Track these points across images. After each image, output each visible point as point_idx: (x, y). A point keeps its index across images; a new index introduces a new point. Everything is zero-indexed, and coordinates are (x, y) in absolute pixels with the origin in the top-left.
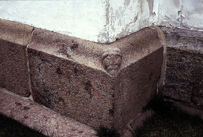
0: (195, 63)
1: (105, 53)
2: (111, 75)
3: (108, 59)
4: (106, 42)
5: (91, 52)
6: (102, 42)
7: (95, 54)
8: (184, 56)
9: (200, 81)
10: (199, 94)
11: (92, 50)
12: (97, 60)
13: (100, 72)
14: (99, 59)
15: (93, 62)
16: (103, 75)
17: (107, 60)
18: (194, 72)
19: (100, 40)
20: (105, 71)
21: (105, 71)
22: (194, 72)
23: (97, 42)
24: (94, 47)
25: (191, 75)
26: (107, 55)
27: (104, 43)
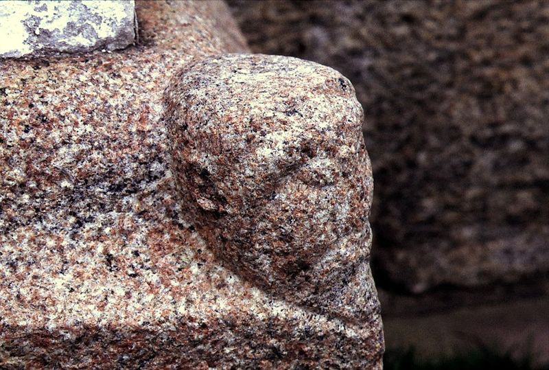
0: (389, 48)
1: (279, 138)
2: (346, 321)
3: (317, 182)
4: (122, 34)
5: (29, 173)
6: (82, 41)
7: (86, 179)
8: (315, 20)
9: (422, 145)
10: (421, 223)
11: (24, 144)
12: (126, 233)
13: (229, 336)
14: (140, 214)
15: (93, 263)
16: (262, 353)
17: (313, 195)
18: (385, 105)
19: (60, 24)
20: (279, 309)
21: (279, 309)
22: (385, 105)
23: (26, 50)
24: (43, 109)
25: (198, 142)
26: (308, 150)
27: (103, 45)
